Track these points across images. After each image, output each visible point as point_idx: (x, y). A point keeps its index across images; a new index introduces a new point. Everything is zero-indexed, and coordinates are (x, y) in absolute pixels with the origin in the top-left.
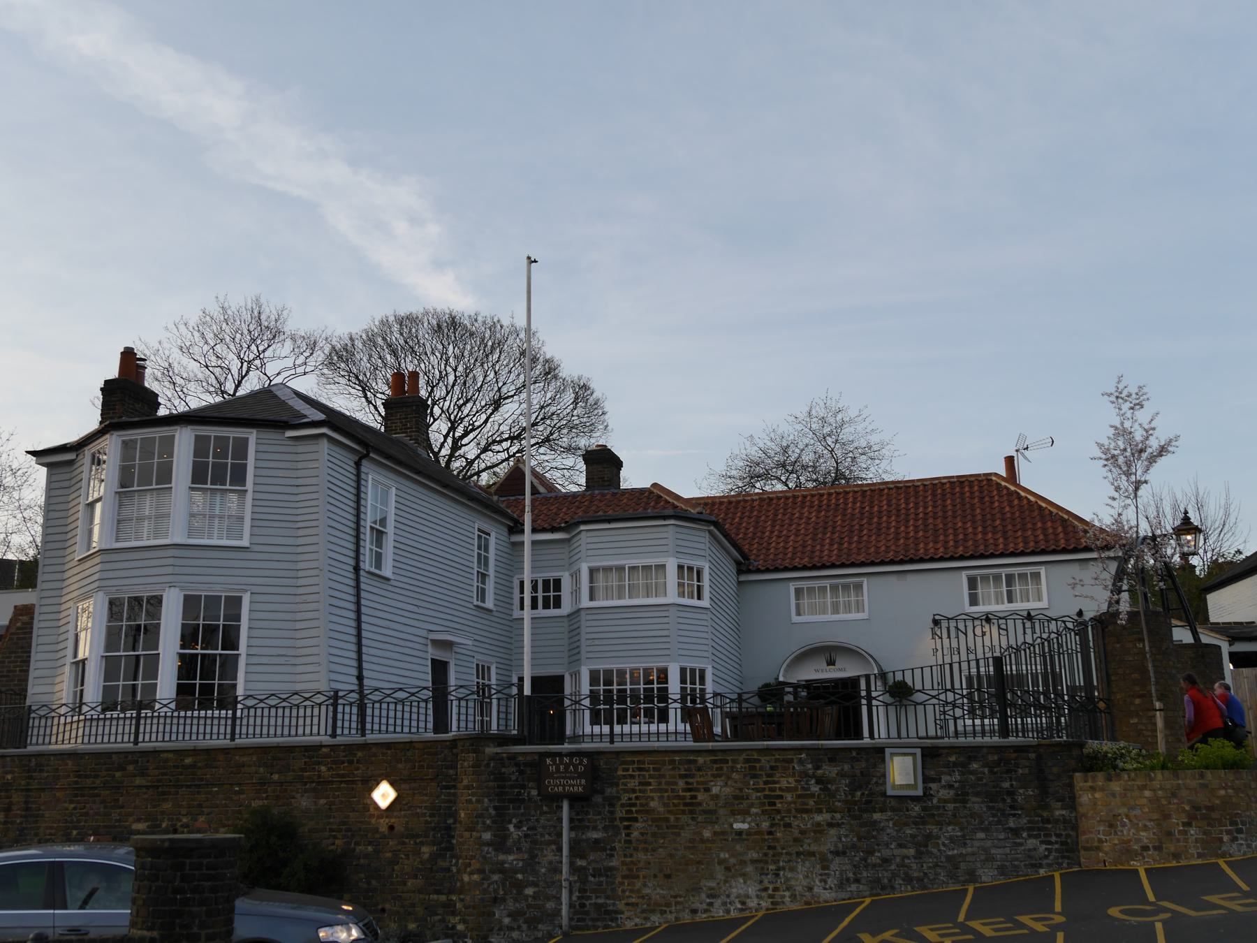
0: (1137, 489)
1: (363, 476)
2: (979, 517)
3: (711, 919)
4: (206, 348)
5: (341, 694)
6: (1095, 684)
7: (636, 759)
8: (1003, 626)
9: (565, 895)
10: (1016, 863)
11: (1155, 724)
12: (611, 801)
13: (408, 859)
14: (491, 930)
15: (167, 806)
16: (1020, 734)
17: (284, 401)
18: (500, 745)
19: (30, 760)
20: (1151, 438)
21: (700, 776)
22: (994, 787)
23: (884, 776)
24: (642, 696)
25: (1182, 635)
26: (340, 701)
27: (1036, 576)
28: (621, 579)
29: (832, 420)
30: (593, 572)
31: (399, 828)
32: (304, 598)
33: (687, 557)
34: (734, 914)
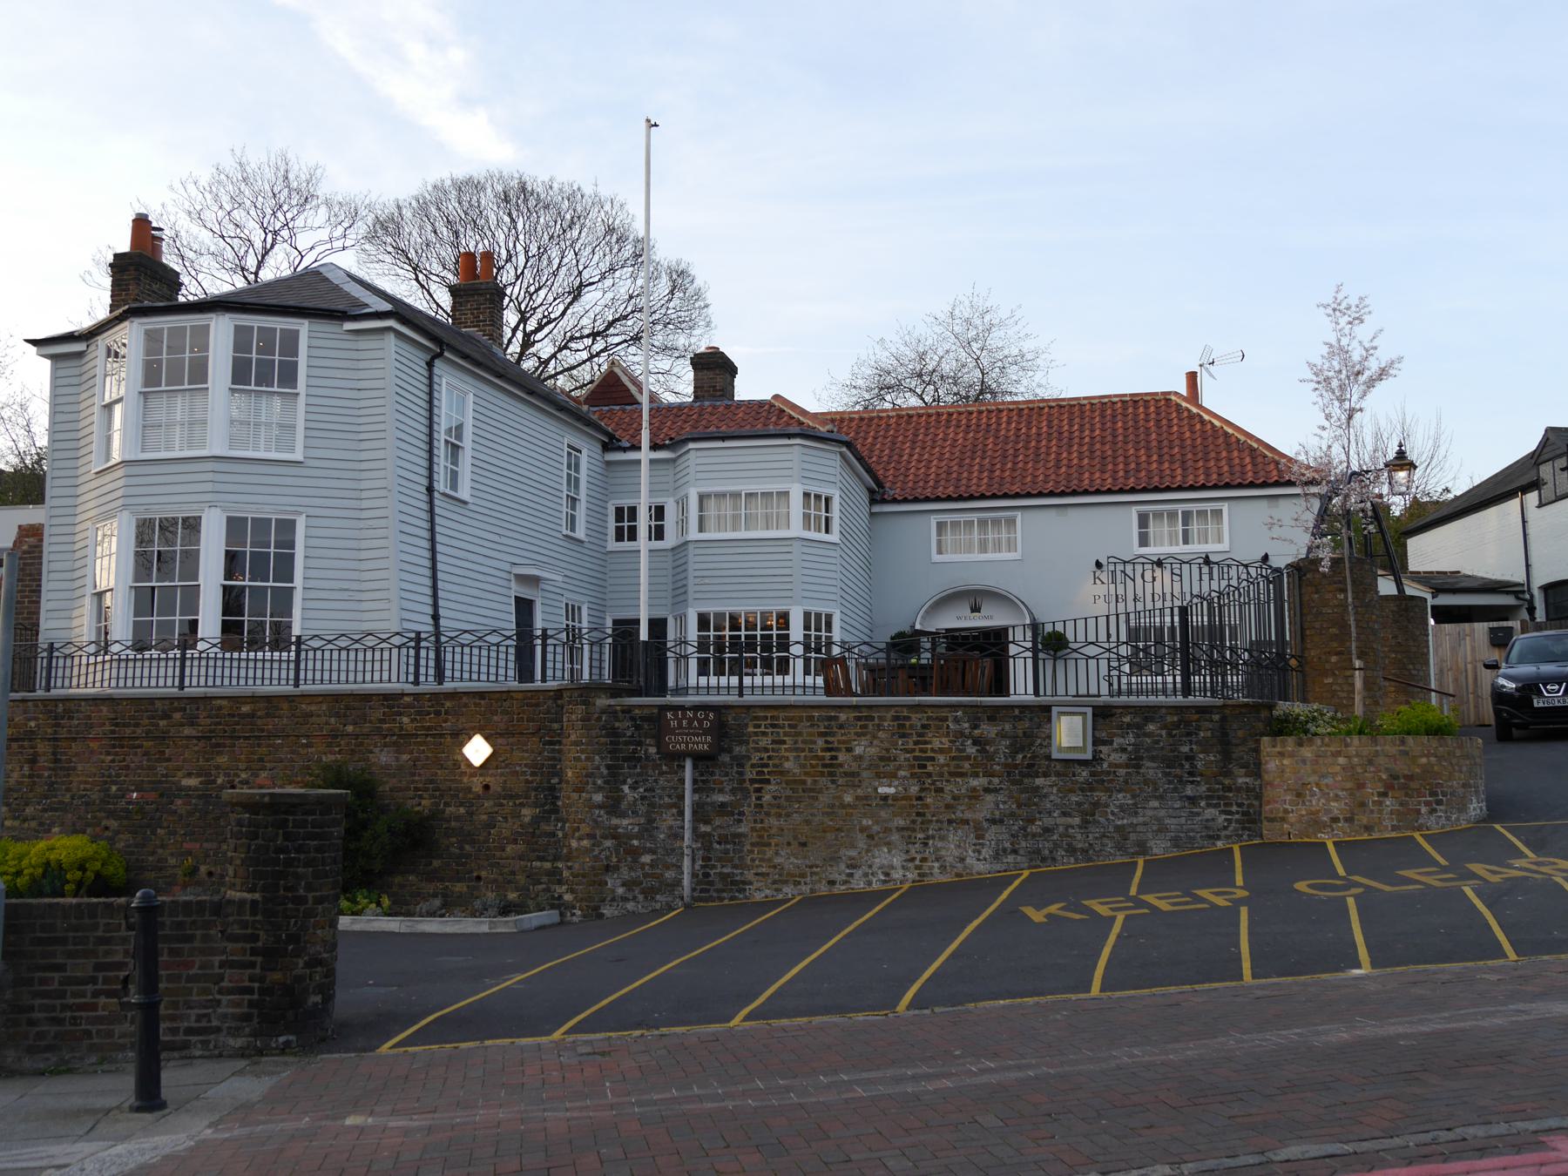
0: (1350, 417)
1: (436, 379)
2: (1154, 443)
4: (221, 214)
5: (423, 636)
6: (1288, 639)
8: (1177, 571)
9: (687, 862)
11: (1353, 685)
12: (740, 762)
13: (506, 821)
14: (603, 900)
15: (222, 760)
16: (1209, 694)
17: (337, 286)
18: (613, 696)
19: (56, 706)
20: (1370, 358)
21: (842, 735)
23: (1049, 737)
24: (727, 644)
25: (1386, 587)
26: (56, 654)
28: (736, 507)
29: (978, 322)
30: (702, 498)
31: (496, 787)
33: (816, 483)
34: (876, 886)
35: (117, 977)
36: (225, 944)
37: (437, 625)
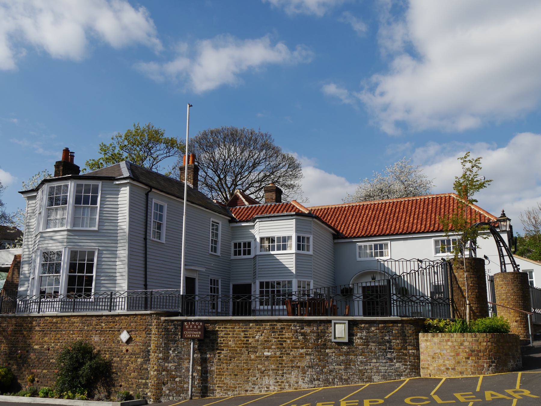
3: (253, 394)
10: (390, 374)
14: (162, 396)
15: (46, 339)
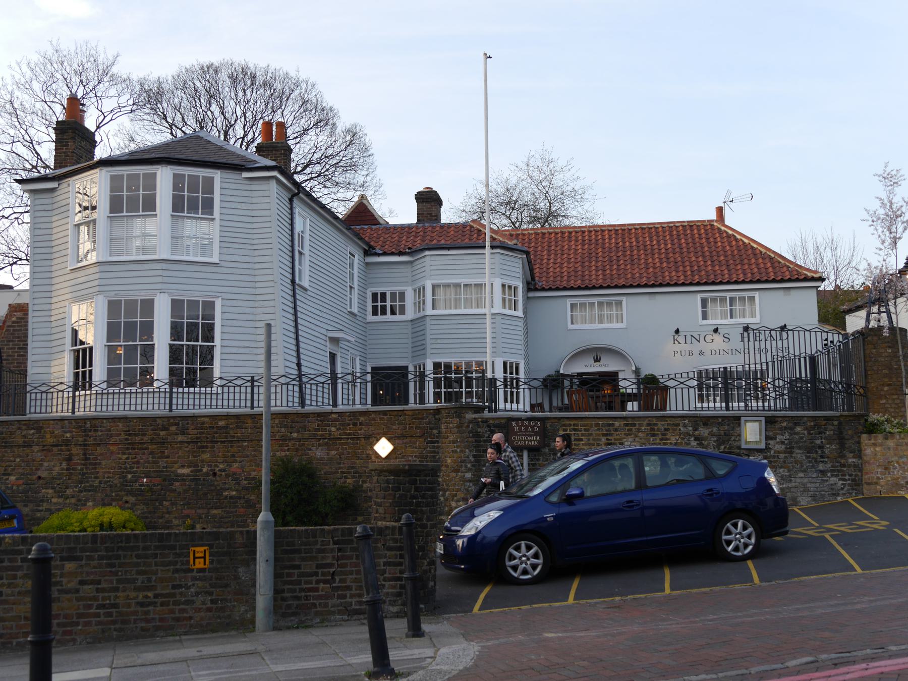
2: (707, 253)
7: (572, 423)
15: (206, 456)
18: (476, 412)
22: (811, 443)
23: (739, 435)
26: (256, 384)
27: (752, 299)
29: (545, 168)
30: (434, 287)
32: (262, 303)
35: (329, 572)
36: (386, 552)
37: (299, 370)
